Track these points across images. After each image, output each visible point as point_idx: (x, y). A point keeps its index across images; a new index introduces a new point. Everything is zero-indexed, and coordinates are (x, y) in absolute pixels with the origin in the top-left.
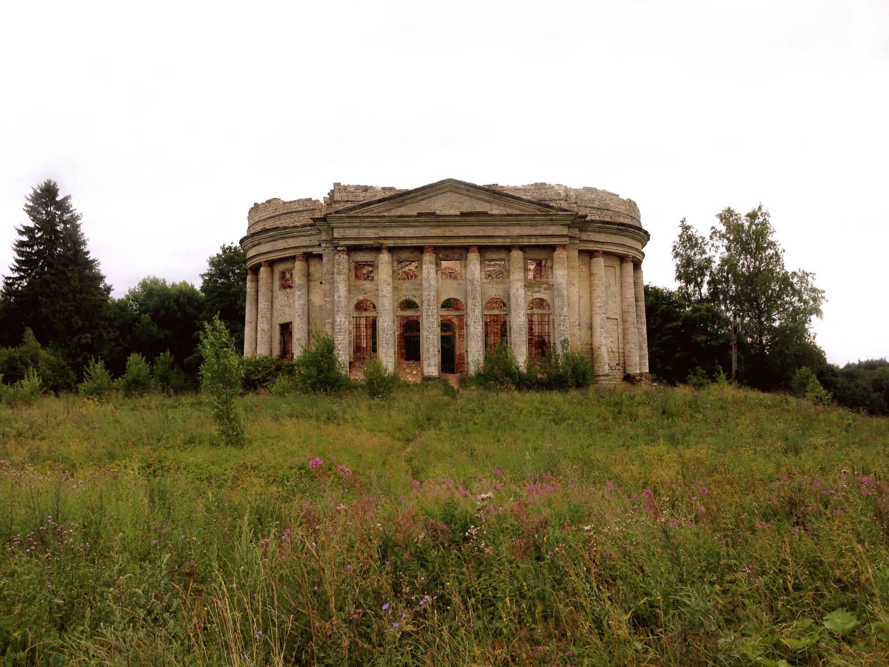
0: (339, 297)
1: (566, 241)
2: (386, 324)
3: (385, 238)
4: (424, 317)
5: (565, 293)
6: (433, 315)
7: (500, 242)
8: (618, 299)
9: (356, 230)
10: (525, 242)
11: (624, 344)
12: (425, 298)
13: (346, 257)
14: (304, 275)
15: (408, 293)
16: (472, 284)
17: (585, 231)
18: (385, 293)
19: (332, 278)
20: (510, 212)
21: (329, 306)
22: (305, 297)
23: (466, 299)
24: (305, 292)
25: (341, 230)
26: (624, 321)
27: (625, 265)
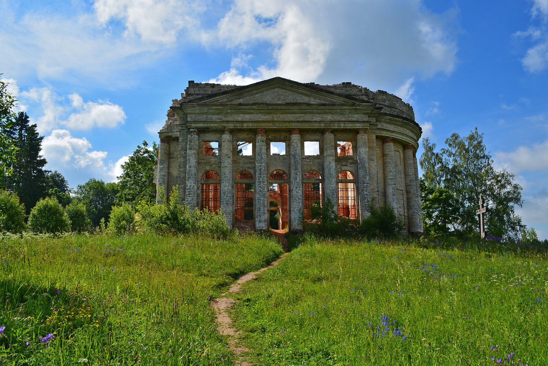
0: (190, 167)
1: (367, 126)
2: (226, 188)
3: (227, 122)
4: (257, 183)
5: (367, 165)
6: (264, 182)
7: (316, 126)
8: (403, 176)
9: (205, 116)
10: (336, 126)
11: (408, 210)
12: (257, 169)
13: (196, 136)
14: (166, 153)
15: (245, 166)
16: (295, 158)
17: (380, 122)
18: (226, 164)
19: (185, 153)
20: (322, 102)
21: (182, 175)
22: (166, 170)
23: (290, 170)
24: (166, 165)
25: (193, 116)
26: (408, 192)
27: (407, 151)
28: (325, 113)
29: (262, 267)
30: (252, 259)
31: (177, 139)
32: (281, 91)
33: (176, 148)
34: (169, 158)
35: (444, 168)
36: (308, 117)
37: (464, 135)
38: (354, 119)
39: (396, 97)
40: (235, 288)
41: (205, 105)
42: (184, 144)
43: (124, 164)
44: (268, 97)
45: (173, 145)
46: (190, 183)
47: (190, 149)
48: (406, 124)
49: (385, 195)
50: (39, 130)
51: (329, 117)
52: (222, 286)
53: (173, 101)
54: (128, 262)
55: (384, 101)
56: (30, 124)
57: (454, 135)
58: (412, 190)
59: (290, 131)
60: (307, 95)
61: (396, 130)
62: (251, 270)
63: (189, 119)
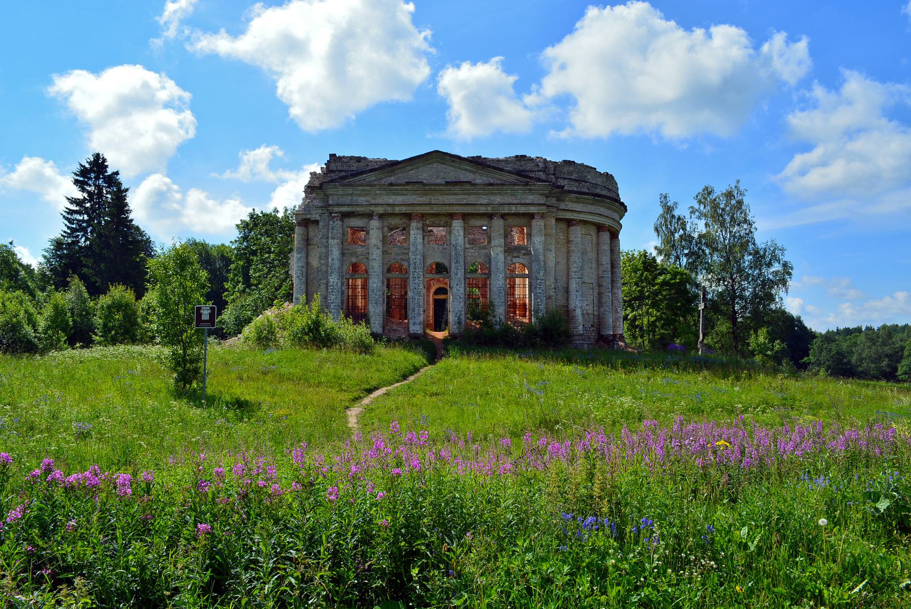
0: (333, 260)
1: (543, 209)
4: (411, 279)
5: (542, 258)
7: (482, 210)
8: (594, 265)
9: (349, 198)
10: (506, 210)
12: (412, 262)
13: (339, 223)
18: (375, 256)
19: (327, 242)
20: (492, 181)
24: (304, 254)
25: (336, 198)
27: (601, 233)
28: (493, 194)
29: (397, 381)
30: (388, 375)
31: (317, 222)
32: (441, 167)
33: (316, 234)
34: (308, 245)
35: (687, 238)
36: (472, 199)
37: (719, 190)
38: (528, 202)
39: (587, 166)
40: (366, 401)
41: (350, 185)
42: (325, 231)
43: (239, 223)
44: (424, 174)
45: (312, 231)
46: (334, 279)
47: (332, 238)
48: (598, 201)
49: (567, 290)
50: (124, 179)
51: (498, 199)
52: (356, 399)
53: (311, 173)
54: (282, 378)
55: (571, 173)
56: (110, 171)
57: (707, 188)
58: (604, 284)
59: (452, 216)
60: (472, 172)
61: (584, 209)
62: (385, 385)
63: (330, 202)
